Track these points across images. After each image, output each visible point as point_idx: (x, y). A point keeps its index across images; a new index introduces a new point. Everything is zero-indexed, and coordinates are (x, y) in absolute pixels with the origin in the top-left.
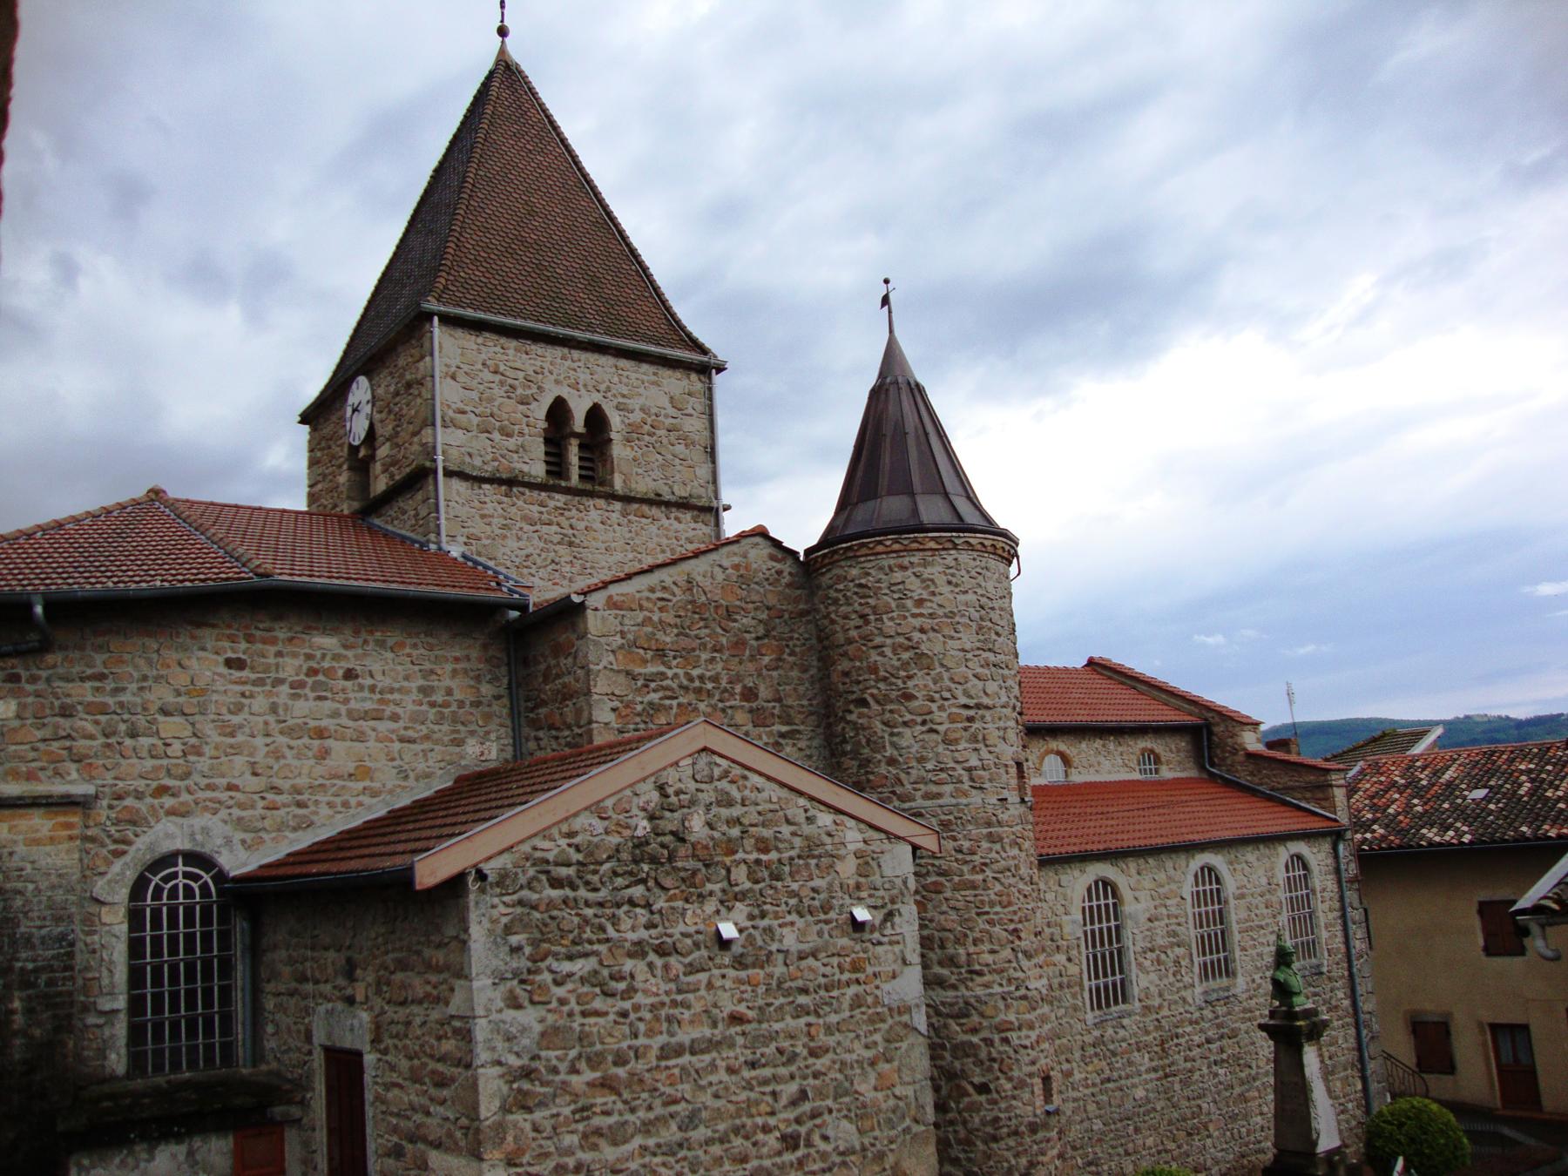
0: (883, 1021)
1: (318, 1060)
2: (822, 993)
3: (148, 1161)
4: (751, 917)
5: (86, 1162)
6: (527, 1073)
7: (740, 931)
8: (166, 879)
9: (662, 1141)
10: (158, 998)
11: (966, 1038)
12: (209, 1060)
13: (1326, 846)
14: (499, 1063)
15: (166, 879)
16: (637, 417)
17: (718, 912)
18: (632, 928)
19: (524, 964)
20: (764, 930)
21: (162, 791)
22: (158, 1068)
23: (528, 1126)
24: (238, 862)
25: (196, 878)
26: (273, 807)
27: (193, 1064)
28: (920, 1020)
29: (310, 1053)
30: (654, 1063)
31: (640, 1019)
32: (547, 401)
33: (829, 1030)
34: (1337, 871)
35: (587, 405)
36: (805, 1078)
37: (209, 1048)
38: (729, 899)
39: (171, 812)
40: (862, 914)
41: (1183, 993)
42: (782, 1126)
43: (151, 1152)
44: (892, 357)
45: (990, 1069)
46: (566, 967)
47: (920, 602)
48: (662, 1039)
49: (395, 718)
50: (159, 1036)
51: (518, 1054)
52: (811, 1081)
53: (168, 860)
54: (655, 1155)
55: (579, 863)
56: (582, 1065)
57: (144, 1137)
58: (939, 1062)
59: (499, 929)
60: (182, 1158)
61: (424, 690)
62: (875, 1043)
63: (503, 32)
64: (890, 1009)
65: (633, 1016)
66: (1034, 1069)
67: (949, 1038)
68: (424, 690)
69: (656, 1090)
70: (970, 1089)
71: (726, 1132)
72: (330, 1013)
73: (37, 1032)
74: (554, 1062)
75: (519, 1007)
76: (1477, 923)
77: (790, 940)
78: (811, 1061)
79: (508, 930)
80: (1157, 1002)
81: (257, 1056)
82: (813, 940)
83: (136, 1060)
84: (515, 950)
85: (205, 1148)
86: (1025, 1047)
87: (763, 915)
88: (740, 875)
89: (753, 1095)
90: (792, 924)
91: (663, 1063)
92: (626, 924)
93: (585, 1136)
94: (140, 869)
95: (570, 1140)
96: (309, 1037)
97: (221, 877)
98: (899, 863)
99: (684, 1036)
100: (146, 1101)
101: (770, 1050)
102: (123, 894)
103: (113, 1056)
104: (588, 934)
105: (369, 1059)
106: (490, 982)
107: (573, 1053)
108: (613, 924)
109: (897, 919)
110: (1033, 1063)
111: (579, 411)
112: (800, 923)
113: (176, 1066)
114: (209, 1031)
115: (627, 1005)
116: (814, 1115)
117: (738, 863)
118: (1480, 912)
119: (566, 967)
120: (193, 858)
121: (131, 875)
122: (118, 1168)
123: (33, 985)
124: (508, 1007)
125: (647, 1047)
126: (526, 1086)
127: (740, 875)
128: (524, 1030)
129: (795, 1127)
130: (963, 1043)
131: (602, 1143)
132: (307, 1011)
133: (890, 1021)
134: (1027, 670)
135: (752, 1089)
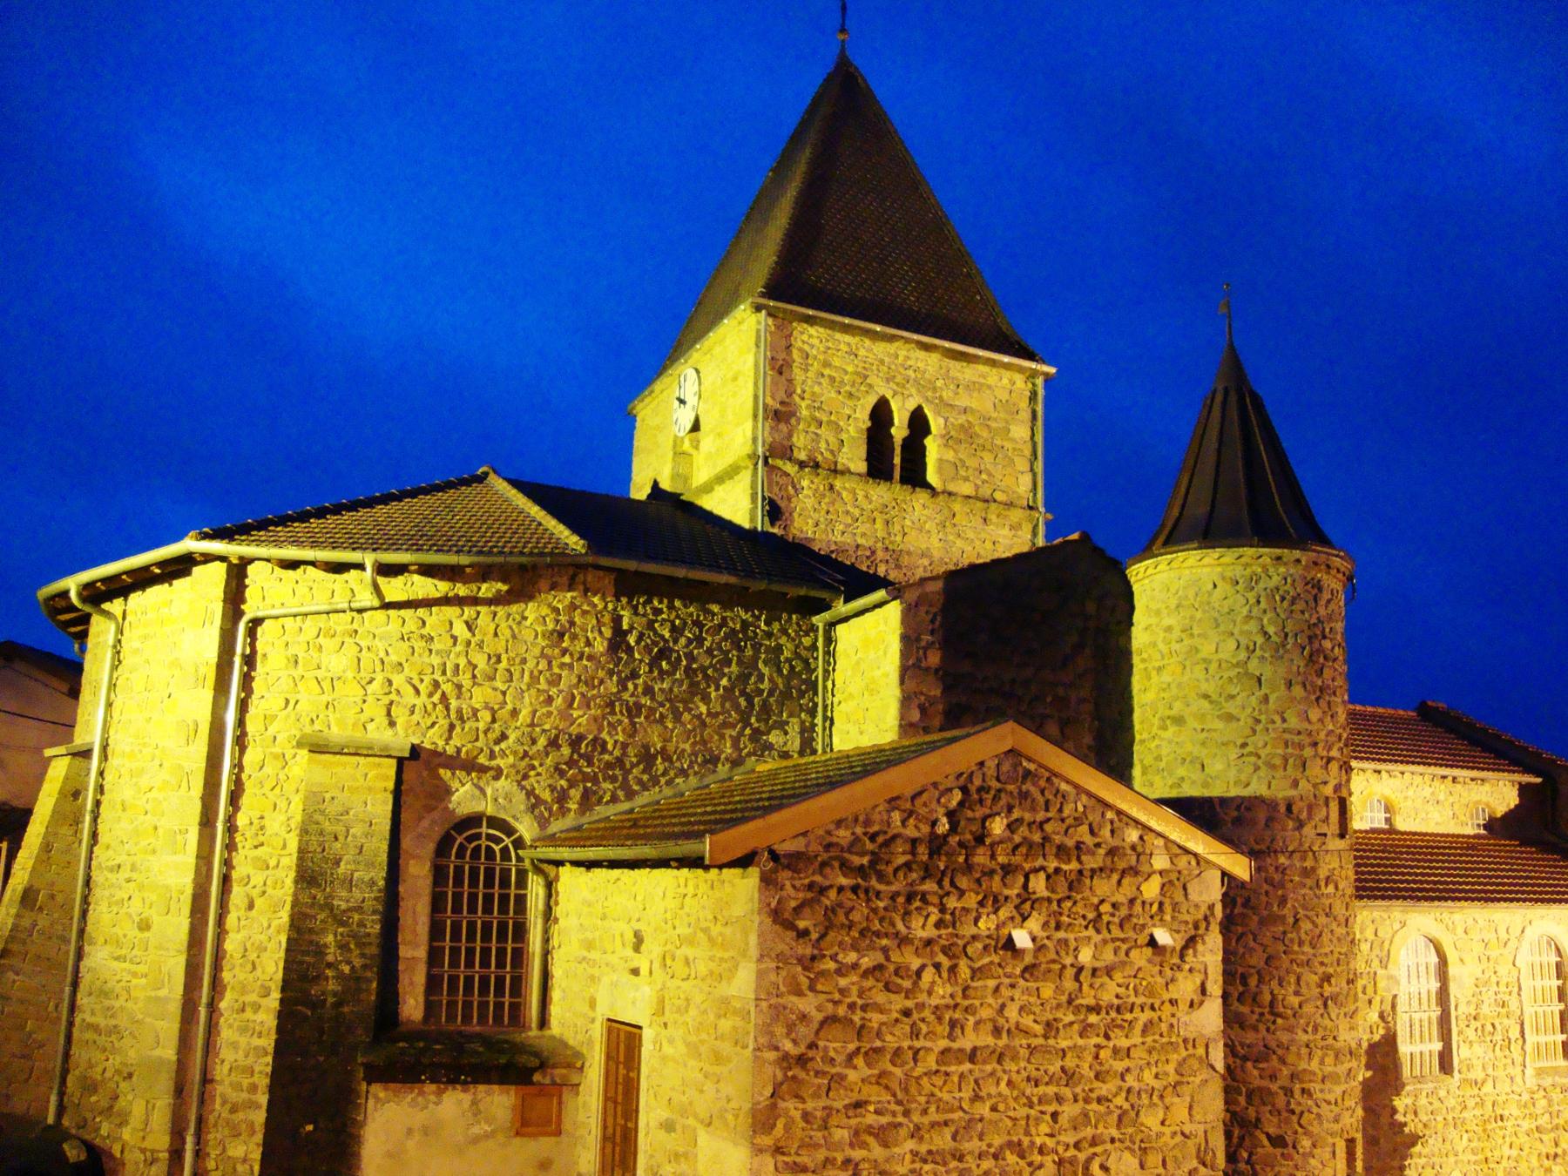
0: (1176, 1050)
1: (598, 1032)
2: (1113, 1014)
3: (437, 1104)
4: (1045, 925)
5: (382, 1095)
6: (802, 1061)
7: (1034, 939)
8: (470, 839)
9: (934, 1148)
10: (455, 952)
11: (1265, 1083)
12: (498, 1017)
14: (777, 1049)
15: (470, 839)
23: (797, 1115)
25: (497, 840)
27: (483, 1018)
28: (1218, 1057)
29: (593, 1021)
31: (923, 1020)
32: (871, 400)
35: (911, 405)
36: (1087, 1101)
37: (499, 1006)
38: (1025, 905)
40: (1163, 937)
42: (1060, 1149)
43: (440, 1093)
45: (1287, 1121)
48: (943, 1043)
51: (795, 1042)
52: (1094, 1106)
54: (925, 1161)
55: (873, 853)
58: (1233, 1108)
60: (466, 1105)
62: (1166, 1074)
64: (1185, 1041)
65: (915, 1016)
66: (1336, 1127)
67: (1244, 1082)
69: (933, 1095)
70: (1266, 1142)
71: (1001, 1147)
72: (614, 985)
74: (832, 1054)
75: (800, 994)
78: (1097, 1084)
80: (1480, 1076)
81: (543, 1022)
85: (489, 1099)
86: (1329, 1103)
87: (1058, 927)
89: (1032, 1112)
90: (1089, 938)
91: (943, 1069)
93: (856, 1133)
95: (842, 1135)
96: (592, 1004)
99: (967, 1042)
101: (1055, 1068)
103: (412, 1001)
104: (876, 926)
105: (648, 1035)
106: (774, 965)
109: (1200, 947)
110: (1336, 1120)
112: (1097, 938)
114: (500, 991)
115: (910, 1004)
116: (1094, 1142)
117: (1036, 871)
120: (494, 822)
122: (410, 1105)
124: (790, 993)
128: (804, 1017)
129: (1072, 1152)
130: (1260, 1089)
131: (871, 1140)
135: (1031, 1107)
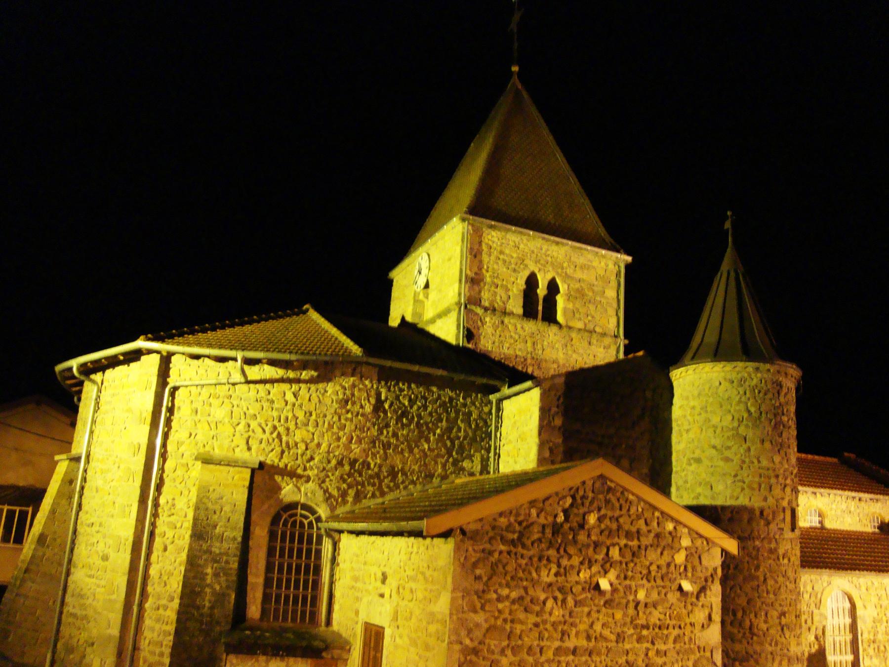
6: (475, 652)
15: (291, 516)
17: (599, 572)
18: (547, 576)
19: (480, 586)
20: (626, 586)
22: (276, 618)
25: (306, 517)
27: (294, 619)
29: (357, 623)
30: (552, 657)
32: (526, 273)
33: (658, 652)
35: (549, 277)
38: (606, 565)
40: (687, 586)
41: (662, 584)
46: (505, 592)
48: (557, 644)
50: (277, 601)
51: (471, 640)
56: (509, 652)
57: (265, 653)
59: (469, 565)
64: (699, 647)
65: (541, 627)
73: (218, 587)
77: (641, 595)
79: (475, 565)
81: (329, 622)
82: (655, 596)
83: (264, 612)
84: (478, 578)
88: (615, 553)
92: (544, 573)
94: (277, 509)
96: (357, 613)
98: (714, 561)
99: (570, 644)
100: (267, 634)
105: (388, 632)
106: (461, 594)
107: (505, 643)
108: (536, 571)
113: (285, 619)
117: (614, 545)
119: (505, 592)
121: (273, 511)
123: (218, 562)
125: (549, 647)
126: (474, 658)
127: (615, 553)
128: (477, 625)
132: (358, 599)
133: (687, 646)
134: (541, 460)
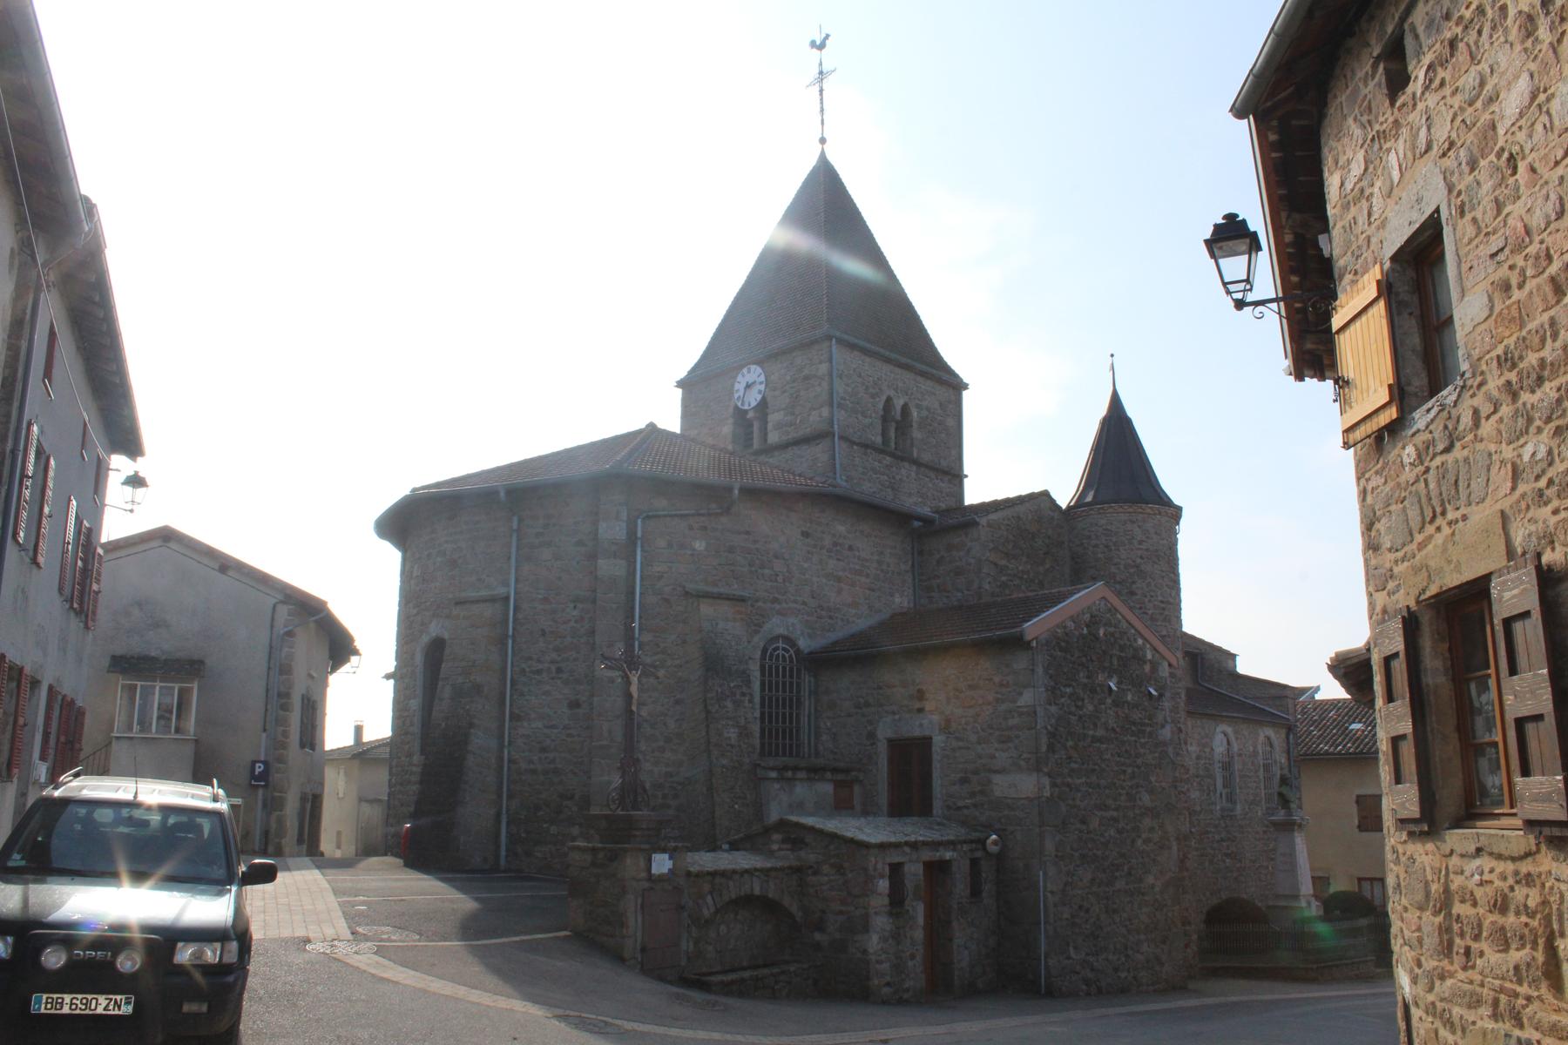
13: (1284, 731)
16: (925, 413)
21: (775, 600)
24: (804, 644)
26: (820, 617)
34: (1288, 752)
39: (779, 613)
44: (1116, 403)
47: (1141, 542)
49: (867, 576)
53: (776, 639)
61: (879, 562)
63: (823, 141)
68: (879, 562)
76: (1354, 809)
97: (798, 651)
102: (758, 654)
111: (899, 403)
118: (1357, 802)
120: (787, 639)
121: (762, 644)
